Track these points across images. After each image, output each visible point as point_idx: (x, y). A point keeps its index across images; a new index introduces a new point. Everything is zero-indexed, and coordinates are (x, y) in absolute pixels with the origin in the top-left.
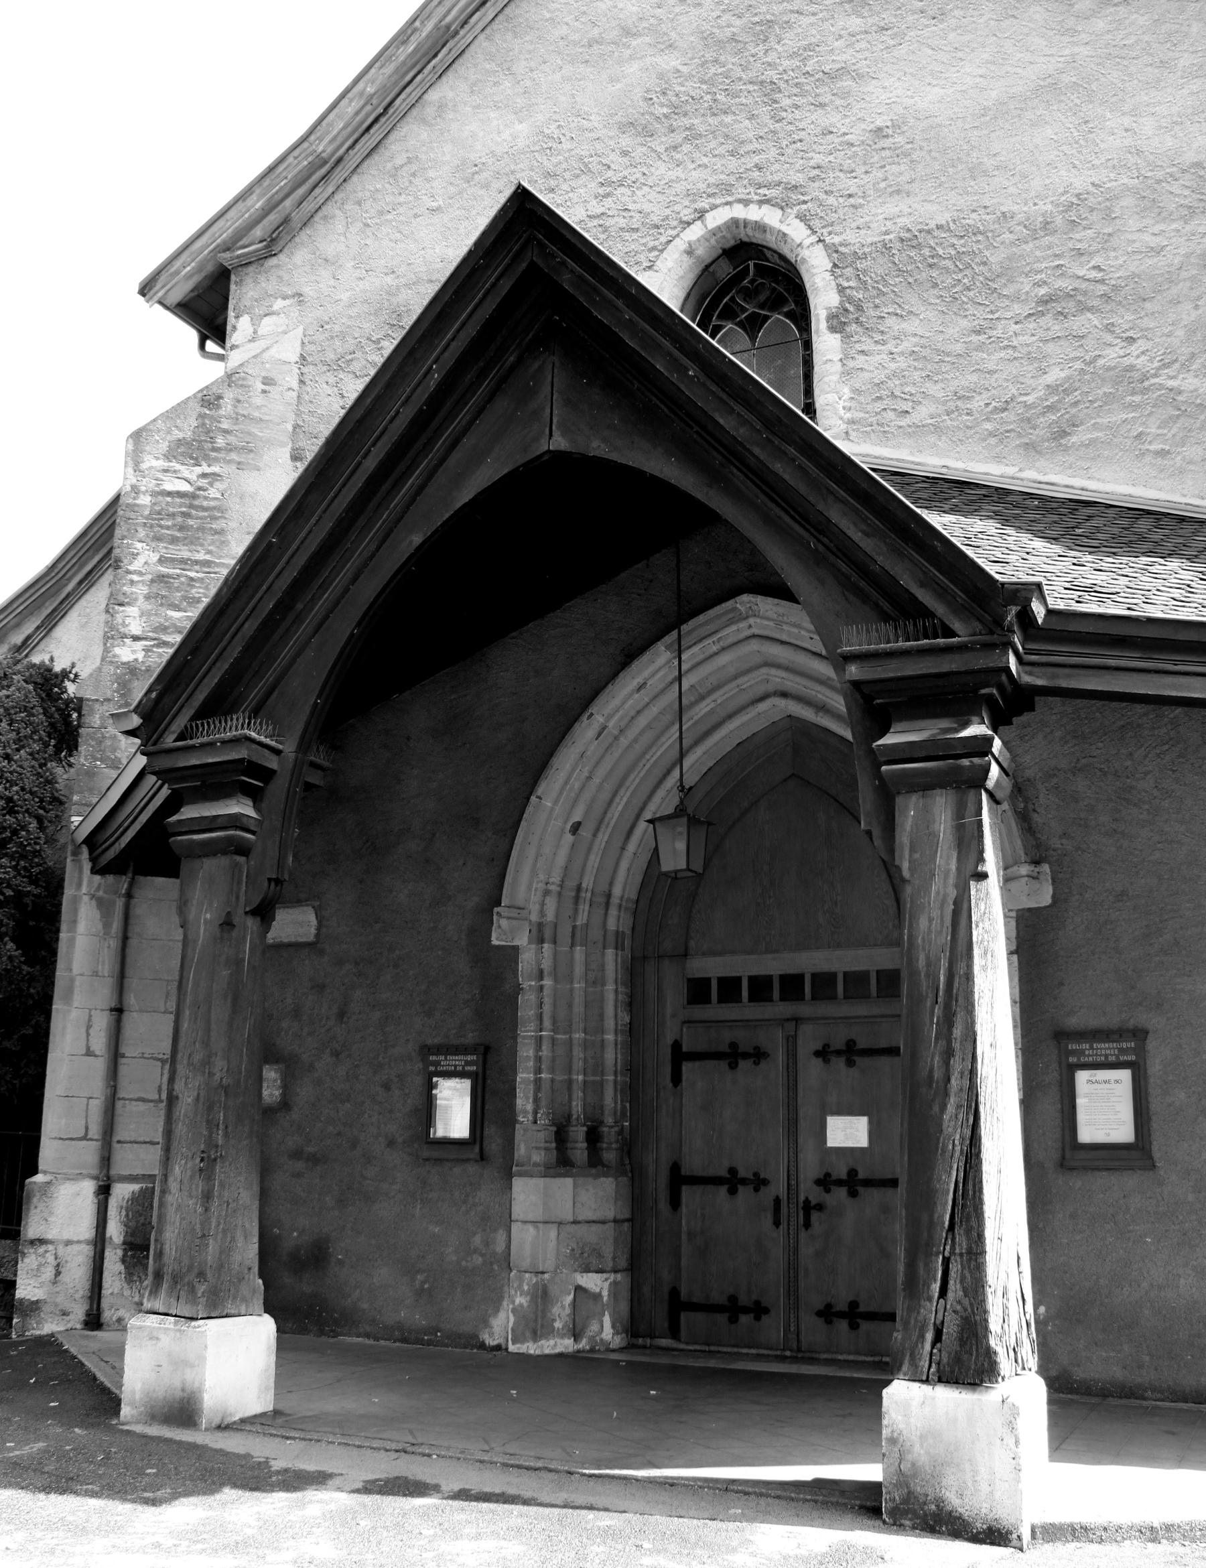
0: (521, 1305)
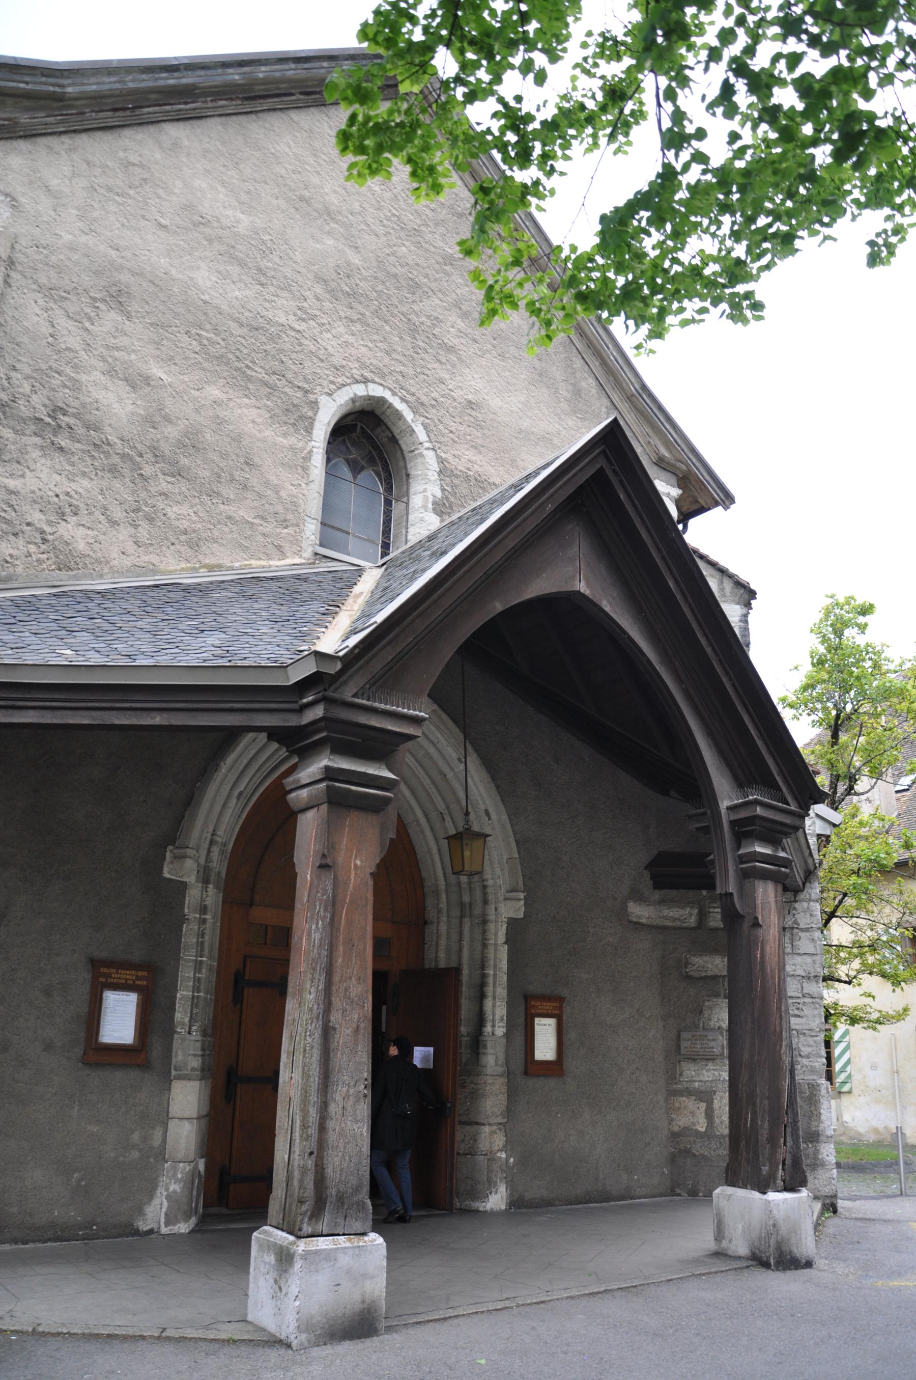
0: (175, 1191)
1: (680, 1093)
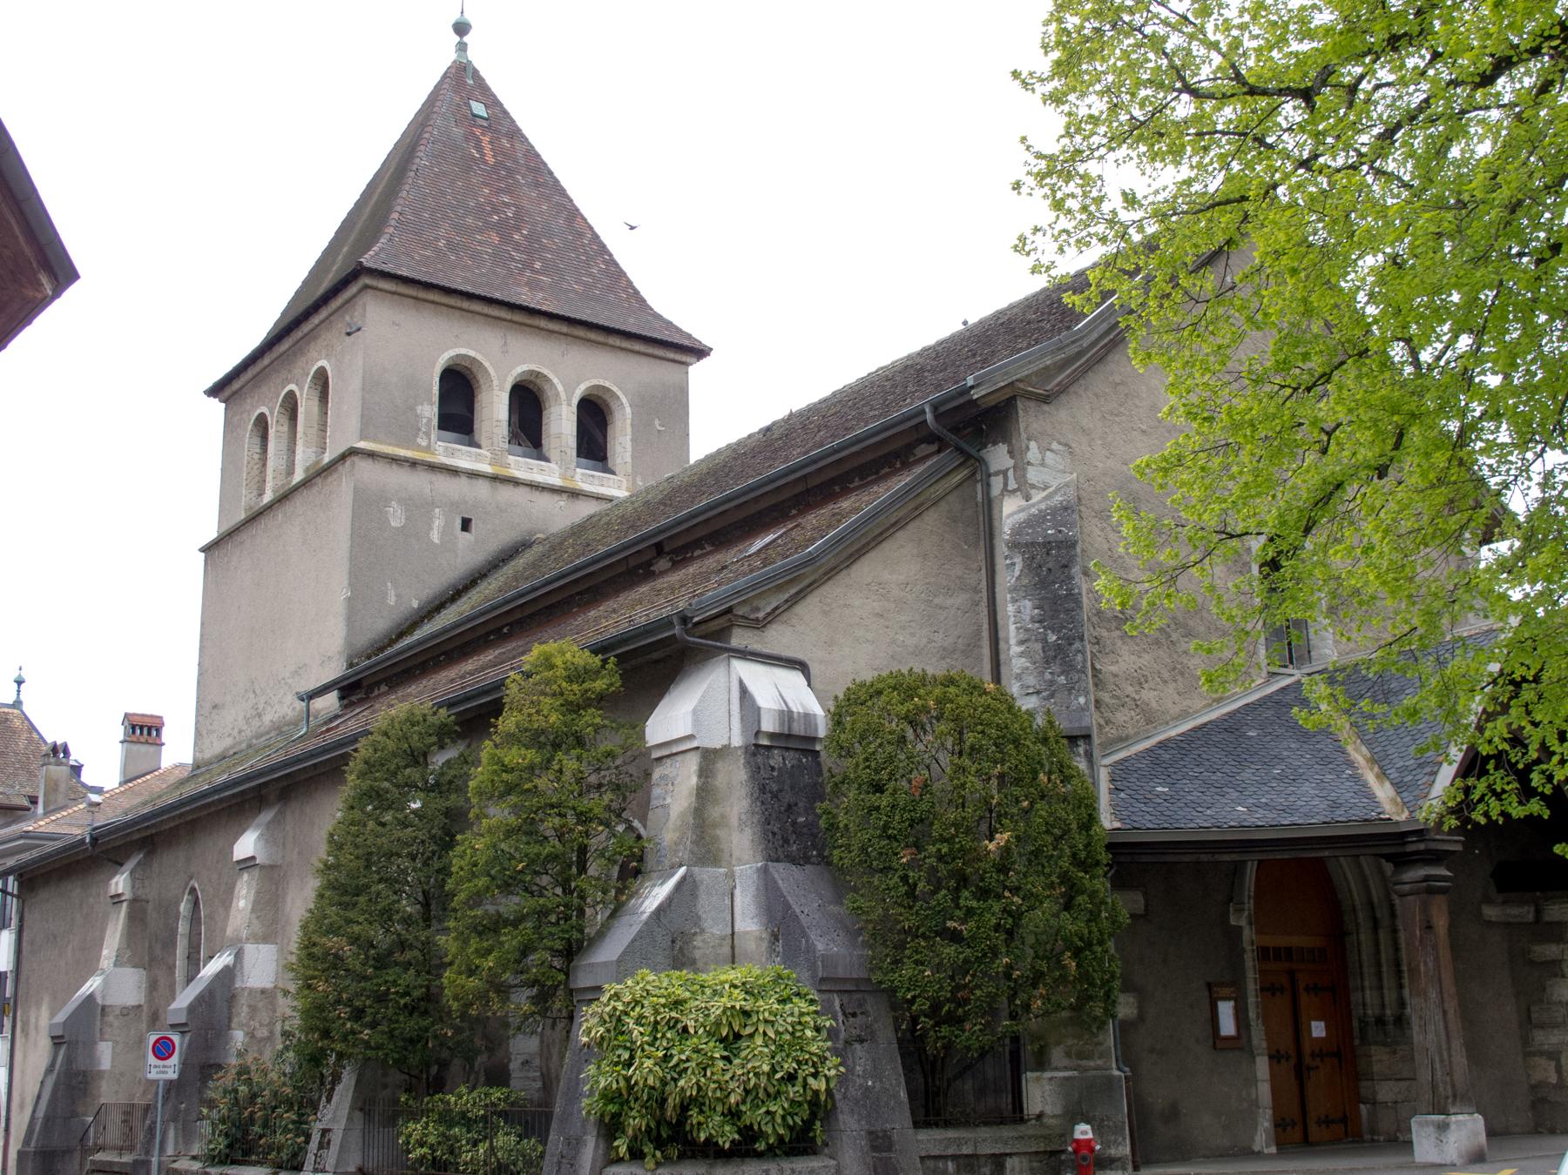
1: (1533, 1054)
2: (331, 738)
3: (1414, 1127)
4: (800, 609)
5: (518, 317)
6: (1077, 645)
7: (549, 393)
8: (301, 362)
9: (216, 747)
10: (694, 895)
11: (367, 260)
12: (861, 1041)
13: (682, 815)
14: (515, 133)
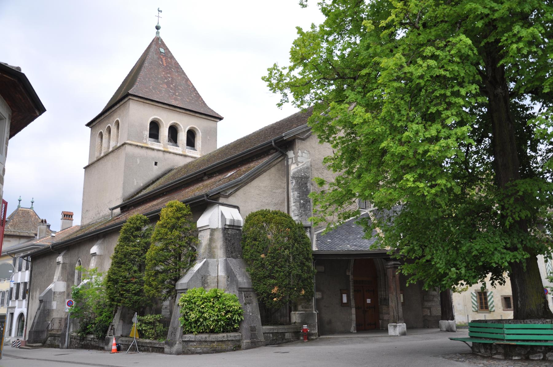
2: (117, 221)
3: (389, 326)
4: (238, 193)
5: (171, 108)
6: (308, 203)
7: (179, 129)
8: (112, 118)
9: (86, 222)
10: (208, 266)
11: (130, 92)
12: (249, 303)
13: (206, 245)
14: (172, 57)
